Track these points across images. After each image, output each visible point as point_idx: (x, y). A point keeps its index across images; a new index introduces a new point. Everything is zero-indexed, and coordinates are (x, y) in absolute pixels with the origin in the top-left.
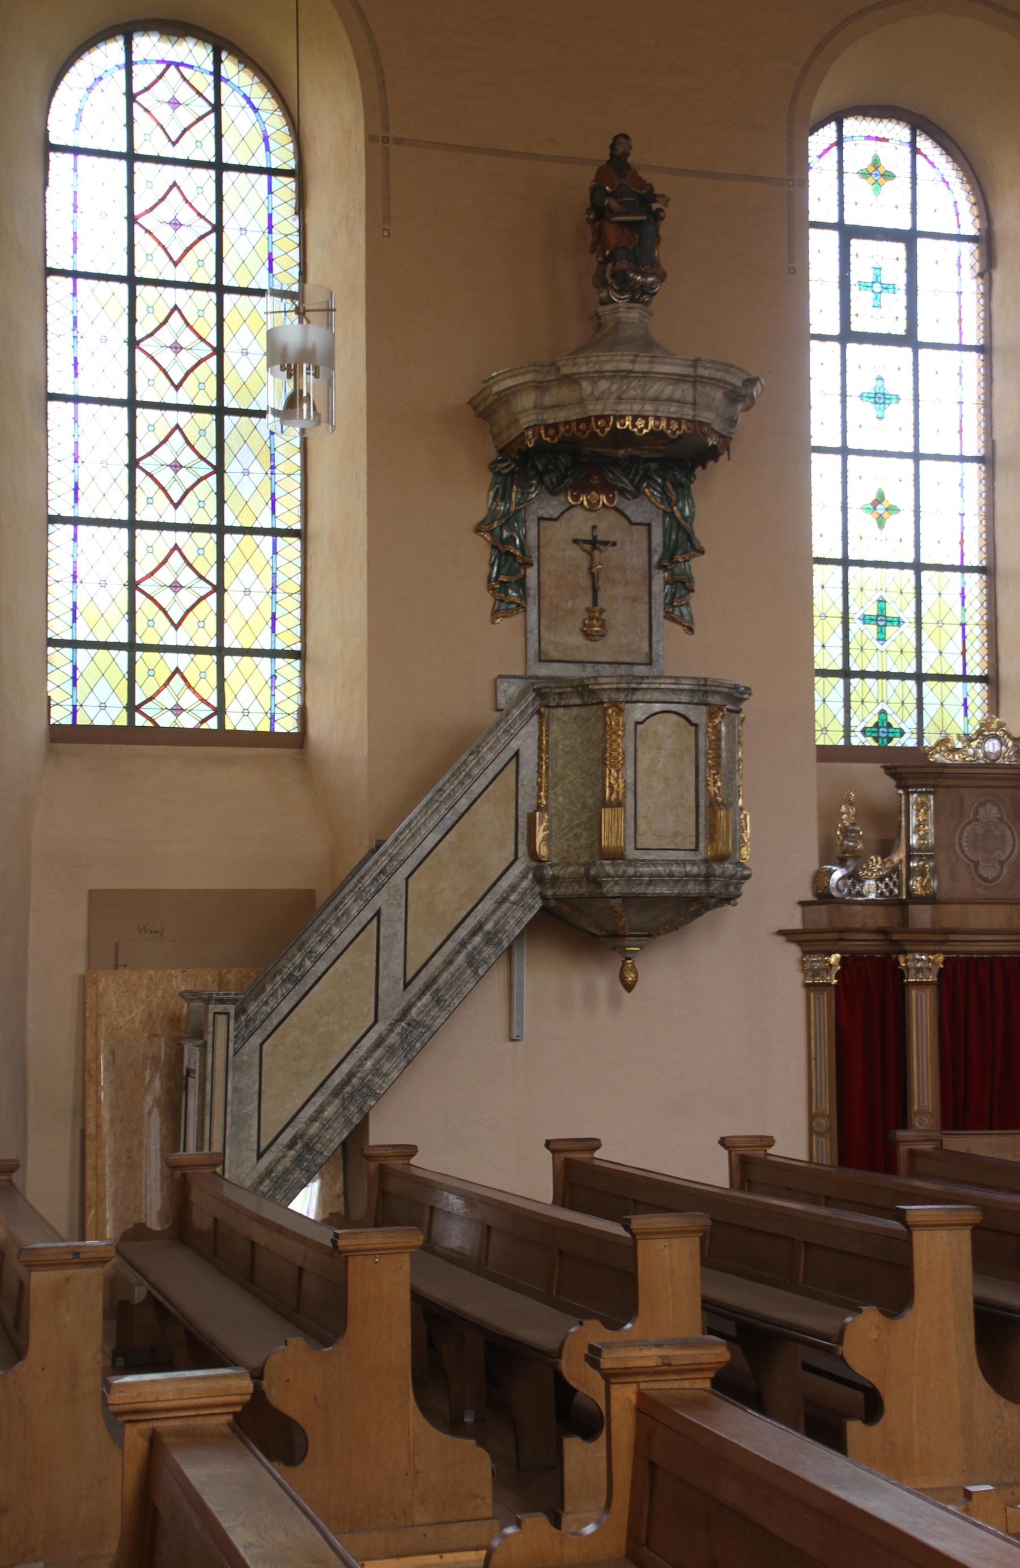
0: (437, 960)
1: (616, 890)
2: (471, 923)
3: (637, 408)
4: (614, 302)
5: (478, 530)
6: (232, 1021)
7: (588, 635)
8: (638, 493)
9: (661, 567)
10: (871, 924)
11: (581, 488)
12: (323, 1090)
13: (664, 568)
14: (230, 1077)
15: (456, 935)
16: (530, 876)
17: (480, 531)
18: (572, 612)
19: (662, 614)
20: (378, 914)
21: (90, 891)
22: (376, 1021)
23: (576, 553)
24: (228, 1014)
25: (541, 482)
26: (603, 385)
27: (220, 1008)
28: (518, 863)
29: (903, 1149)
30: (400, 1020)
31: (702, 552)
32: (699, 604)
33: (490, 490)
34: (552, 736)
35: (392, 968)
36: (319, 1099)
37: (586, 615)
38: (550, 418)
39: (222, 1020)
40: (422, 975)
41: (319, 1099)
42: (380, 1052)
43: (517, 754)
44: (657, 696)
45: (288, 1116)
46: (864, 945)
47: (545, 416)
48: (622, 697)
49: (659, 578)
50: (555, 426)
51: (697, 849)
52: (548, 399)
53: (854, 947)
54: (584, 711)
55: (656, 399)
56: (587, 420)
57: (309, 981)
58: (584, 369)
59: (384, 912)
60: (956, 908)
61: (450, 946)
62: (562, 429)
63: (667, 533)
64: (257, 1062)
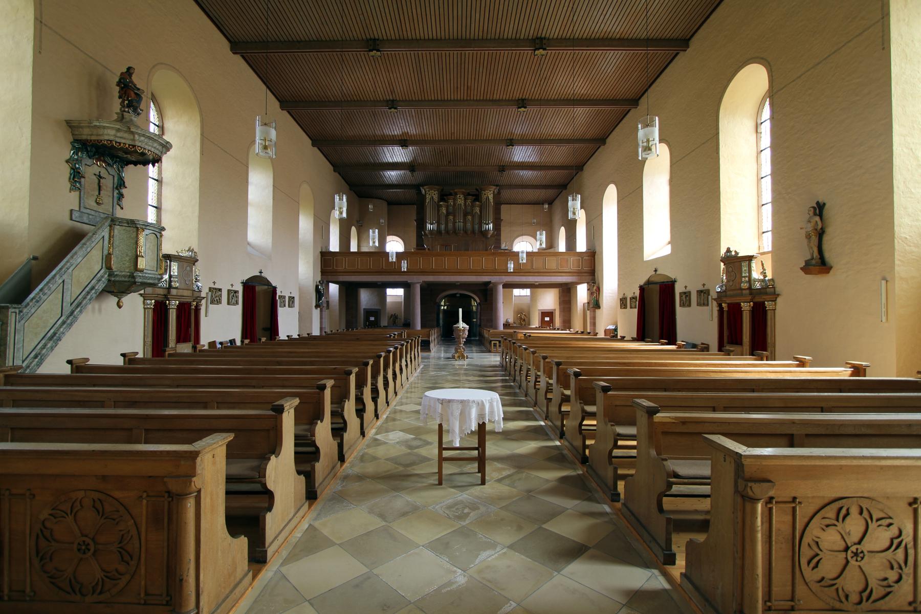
0: (80, 297)
1: (140, 280)
2: (90, 286)
3: (150, 148)
4: (129, 113)
5: (67, 161)
6: (17, 315)
7: (98, 204)
8: (112, 166)
9: (117, 188)
10: (162, 293)
11: (98, 160)
12: (45, 338)
13: (118, 189)
14: (16, 335)
15: (86, 289)
16: (108, 273)
17: (69, 162)
18: (93, 195)
19: (116, 203)
20: (63, 281)
21: (697, 305)
22: (62, 316)
23: (94, 177)
24: (16, 313)
25: (87, 153)
26: (142, 138)
27: (13, 310)
28: (103, 269)
29: (198, 349)
30: (71, 315)
31: (126, 188)
32: (124, 202)
33: (71, 150)
34: (115, 234)
35: (68, 299)
36: (43, 342)
37: (97, 197)
38: (118, 140)
39: (14, 314)
40: (76, 301)
41: (43, 342)
42: (64, 326)
43: (103, 237)
44: (152, 229)
45: (33, 347)
46: (160, 299)
47: (117, 139)
48: (144, 227)
49: (116, 192)
50: (120, 143)
51: (157, 271)
52: (119, 134)
53: (157, 299)
54: (128, 228)
55: (155, 148)
56: (134, 146)
57: (41, 302)
58: (139, 132)
59: (65, 280)
60: (181, 291)
61: (84, 293)
62: (122, 145)
63: (118, 180)
64: (23, 329)
